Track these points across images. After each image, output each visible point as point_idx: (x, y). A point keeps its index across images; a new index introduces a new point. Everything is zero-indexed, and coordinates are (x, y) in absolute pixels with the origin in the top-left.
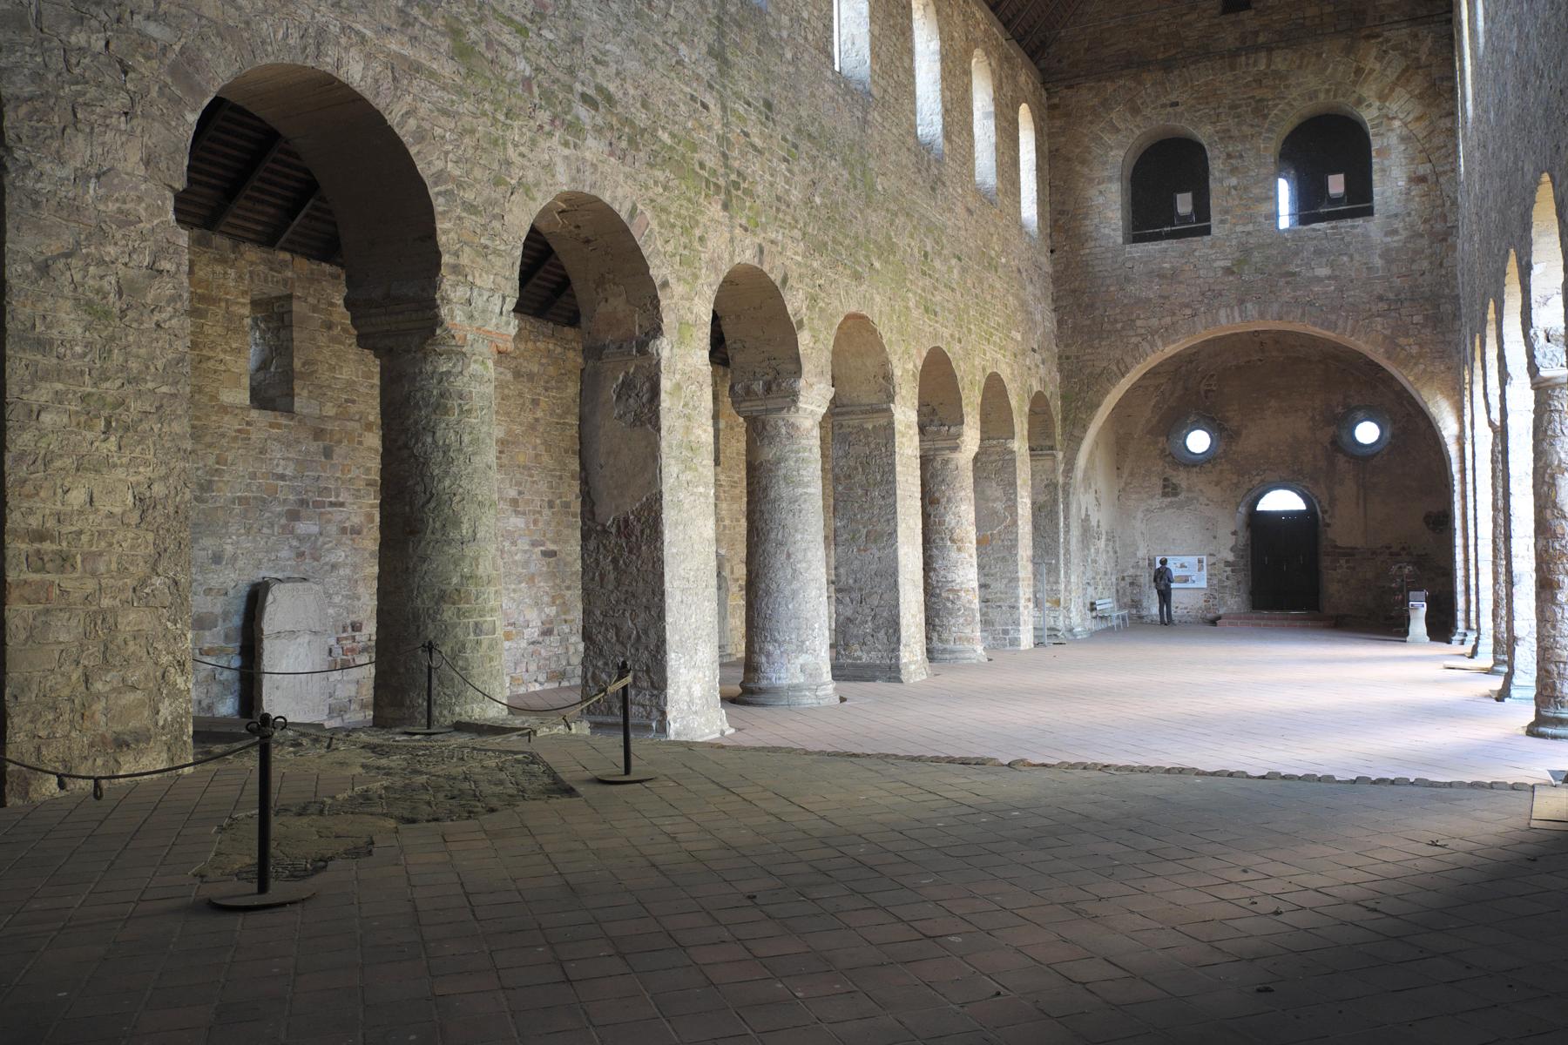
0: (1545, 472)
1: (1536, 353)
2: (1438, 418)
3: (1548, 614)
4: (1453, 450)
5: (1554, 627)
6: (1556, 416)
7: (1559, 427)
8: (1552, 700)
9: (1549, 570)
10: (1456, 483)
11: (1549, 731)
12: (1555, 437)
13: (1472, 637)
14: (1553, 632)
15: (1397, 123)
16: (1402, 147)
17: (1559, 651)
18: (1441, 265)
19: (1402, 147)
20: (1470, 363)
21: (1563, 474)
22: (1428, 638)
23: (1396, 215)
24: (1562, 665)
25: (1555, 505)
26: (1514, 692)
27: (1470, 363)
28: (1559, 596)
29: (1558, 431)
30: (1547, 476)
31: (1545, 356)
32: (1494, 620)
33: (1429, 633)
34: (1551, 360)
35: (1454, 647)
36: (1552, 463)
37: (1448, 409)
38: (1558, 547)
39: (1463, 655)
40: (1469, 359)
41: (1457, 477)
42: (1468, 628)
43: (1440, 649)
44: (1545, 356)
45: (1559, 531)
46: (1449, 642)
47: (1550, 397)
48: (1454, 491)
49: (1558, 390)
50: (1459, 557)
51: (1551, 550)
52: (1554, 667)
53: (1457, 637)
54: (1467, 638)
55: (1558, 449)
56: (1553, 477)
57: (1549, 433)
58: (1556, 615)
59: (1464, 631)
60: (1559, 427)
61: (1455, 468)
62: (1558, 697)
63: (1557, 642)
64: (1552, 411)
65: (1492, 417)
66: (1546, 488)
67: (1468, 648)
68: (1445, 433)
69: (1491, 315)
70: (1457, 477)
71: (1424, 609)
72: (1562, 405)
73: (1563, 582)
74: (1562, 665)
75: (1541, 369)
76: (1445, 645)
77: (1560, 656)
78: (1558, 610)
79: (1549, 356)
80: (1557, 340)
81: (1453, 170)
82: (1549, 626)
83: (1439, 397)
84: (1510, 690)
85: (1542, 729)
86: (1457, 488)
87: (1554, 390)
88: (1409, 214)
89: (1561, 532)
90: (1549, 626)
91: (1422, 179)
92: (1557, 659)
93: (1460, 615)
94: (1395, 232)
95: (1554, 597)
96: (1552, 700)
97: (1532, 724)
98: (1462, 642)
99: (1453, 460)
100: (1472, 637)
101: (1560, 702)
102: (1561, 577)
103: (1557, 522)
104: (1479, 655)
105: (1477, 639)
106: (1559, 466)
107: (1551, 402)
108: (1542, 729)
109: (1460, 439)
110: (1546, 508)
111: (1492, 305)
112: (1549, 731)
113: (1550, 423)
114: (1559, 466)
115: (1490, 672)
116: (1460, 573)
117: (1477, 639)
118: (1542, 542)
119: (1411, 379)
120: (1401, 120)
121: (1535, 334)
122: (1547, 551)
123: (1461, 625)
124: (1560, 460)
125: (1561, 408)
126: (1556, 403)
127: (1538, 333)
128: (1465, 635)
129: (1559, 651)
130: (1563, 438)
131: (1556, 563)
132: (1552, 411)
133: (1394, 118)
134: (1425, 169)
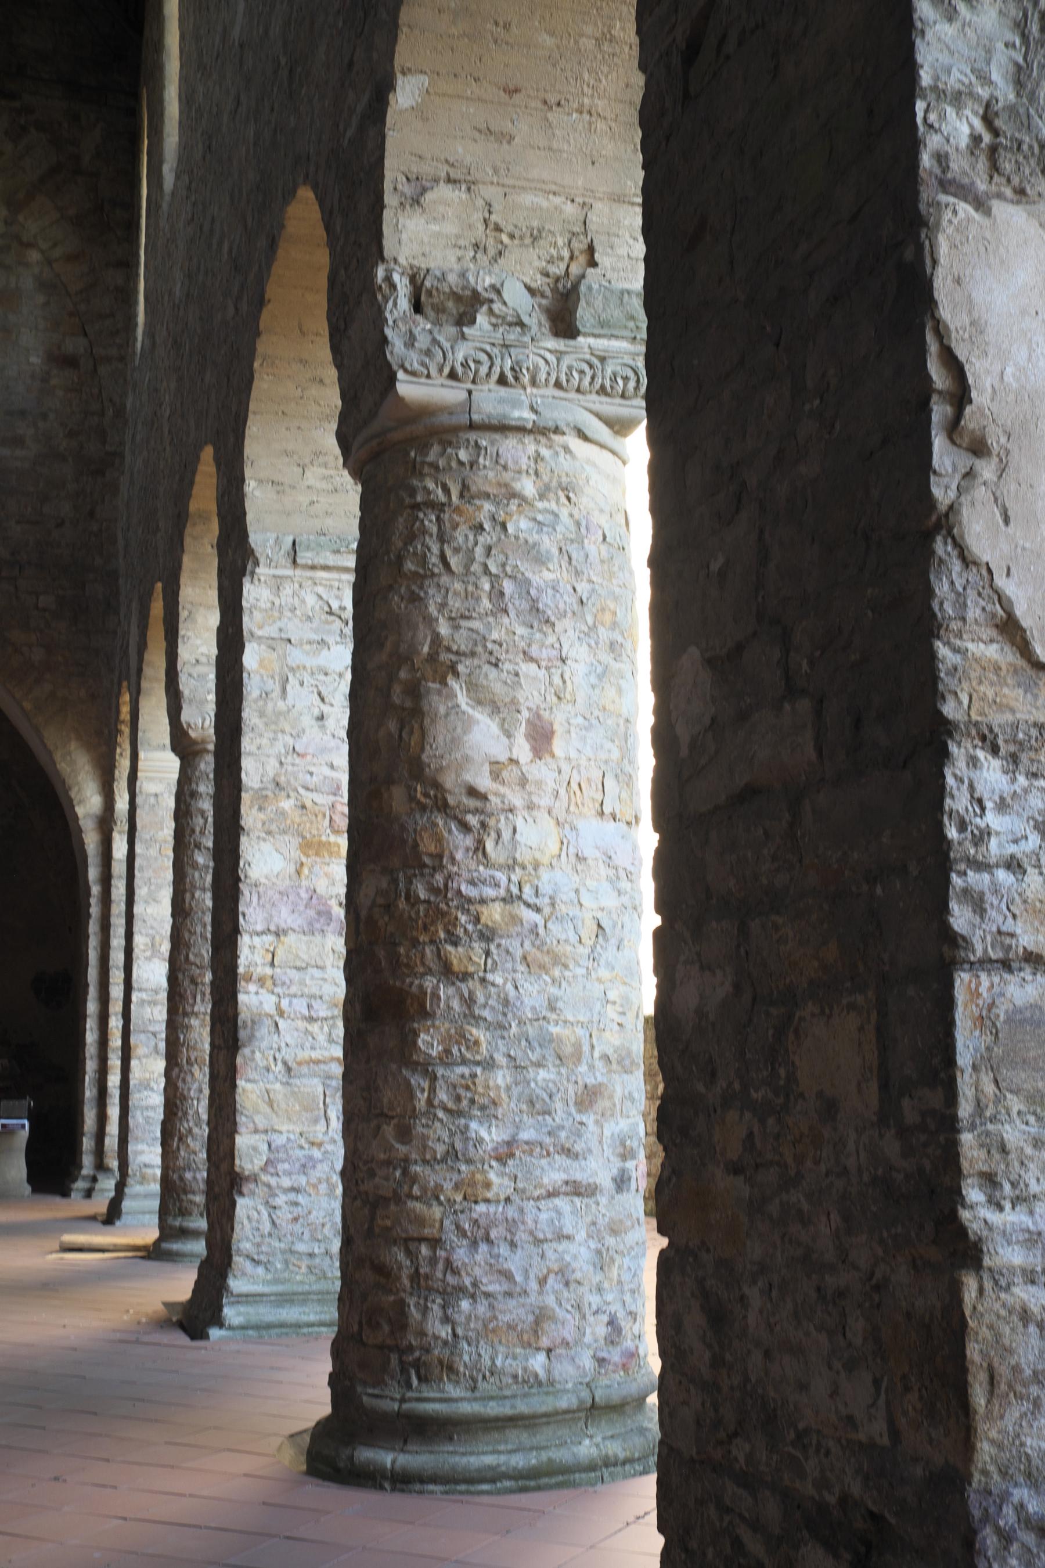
0: (392, 678)
1: (388, 332)
2: (69, 781)
3: (387, 1095)
4: (91, 841)
5: (405, 1134)
6: (430, 522)
7: (435, 549)
8: (394, 1359)
9: (396, 963)
10: (93, 901)
11: (387, 1458)
12: (425, 575)
13: (107, 1185)
14: (402, 1149)
15: (34, 256)
16: (41, 299)
17: (418, 1206)
18: (92, 514)
19: (41, 299)
20: (133, 678)
21: (444, 682)
22: (28, 1189)
23: (23, 413)
24: (424, 1250)
25: (417, 770)
26: (231, 1313)
27: (133, 678)
28: (423, 1039)
29: (434, 560)
30: (397, 689)
31: (411, 341)
32: (164, 1144)
33: (30, 1180)
34: (428, 353)
35: (76, 1205)
36: (414, 650)
37: (88, 767)
38: (423, 895)
39: (93, 1218)
40: (133, 671)
41: (95, 890)
42: (100, 1166)
43: (53, 1208)
44: (411, 341)
45: (428, 846)
46: (65, 1193)
47: (415, 470)
48: (89, 916)
49: (436, 449)
50: (91, 1037)
51: (402, 904)
52: (401, 1256)
53: (80, 1185)
54: (98, 1186)
55: (433, 609)
56: (415, 692)
57: (410, 566)
58: (411, 1096)
59: (91, 1173)
60: (435, 549)
61: (93, 873)
62: (410, 1348)
63: (414, 1179)
64: (416, 507)
65: (187, 715)
66: (392, 726)
67: (100, 1204)
68: (80, 811)
69: (157, 608)
70: (95, 890)
71: (25, 1133)
72: (446, 490)
73: (436, 996)
74: (424, 1250)
75: (401, 375)
76: (58, 1200)
77: (421, 1221)
78: (417, 1081)
79: (423, 341)
80: (440, 310)
81: (122, 359)
82: (389, 1130)
83: (73, 745)
84: (220, 1308)
85: (366, 1454)
86: (95, 910)
87: (424, 448)
88: (44, 416)
89: (432, 848)
90: (389, 1130)
91: (69, 362)
92: (413, 1231)
93: (87, 1143)
94: (18, 441)
95: (408, 1040)
96: (394, 1359)
97: (323, 1430)
98: (89, 1194)
99: (90, 860)
100: (107, 1185)
101: (417, 1365)
102: (429, 982)
103: (422, 821)
104: (124, 1217)
105: (121, 1187)
106: (433, 657)
107: (415, 482)
108: (366, 1454)
109: (106, 822)
110: (390, 782)
111: (126, 698)
112: (387, 1458)
113: (411, 537)
114: (433, 657)
115: (154, 1253)
116: (91, 1066)
117: (121, 1187)
118: (373, 884)
119: (27, 705)
120: (42, 252)
121: (388, 279)
122: (389, 907)
123: (87, 1161)
124: (437, 640)
125: (442, 497)
126: (431, 485)
127: (396, 277)
128: (94, 1179)
129: (418, 1206)
130: (445, 579)
131: (415, 943)
132: (416, 507)
133: (30, 245)
134: (74, 345)
